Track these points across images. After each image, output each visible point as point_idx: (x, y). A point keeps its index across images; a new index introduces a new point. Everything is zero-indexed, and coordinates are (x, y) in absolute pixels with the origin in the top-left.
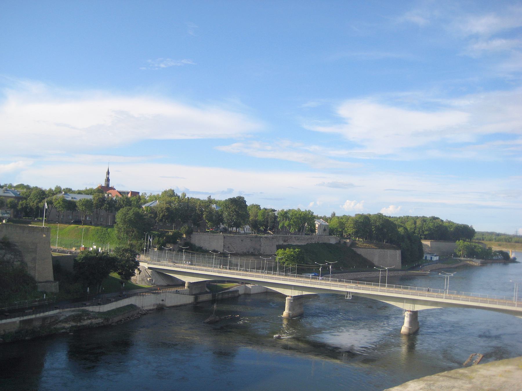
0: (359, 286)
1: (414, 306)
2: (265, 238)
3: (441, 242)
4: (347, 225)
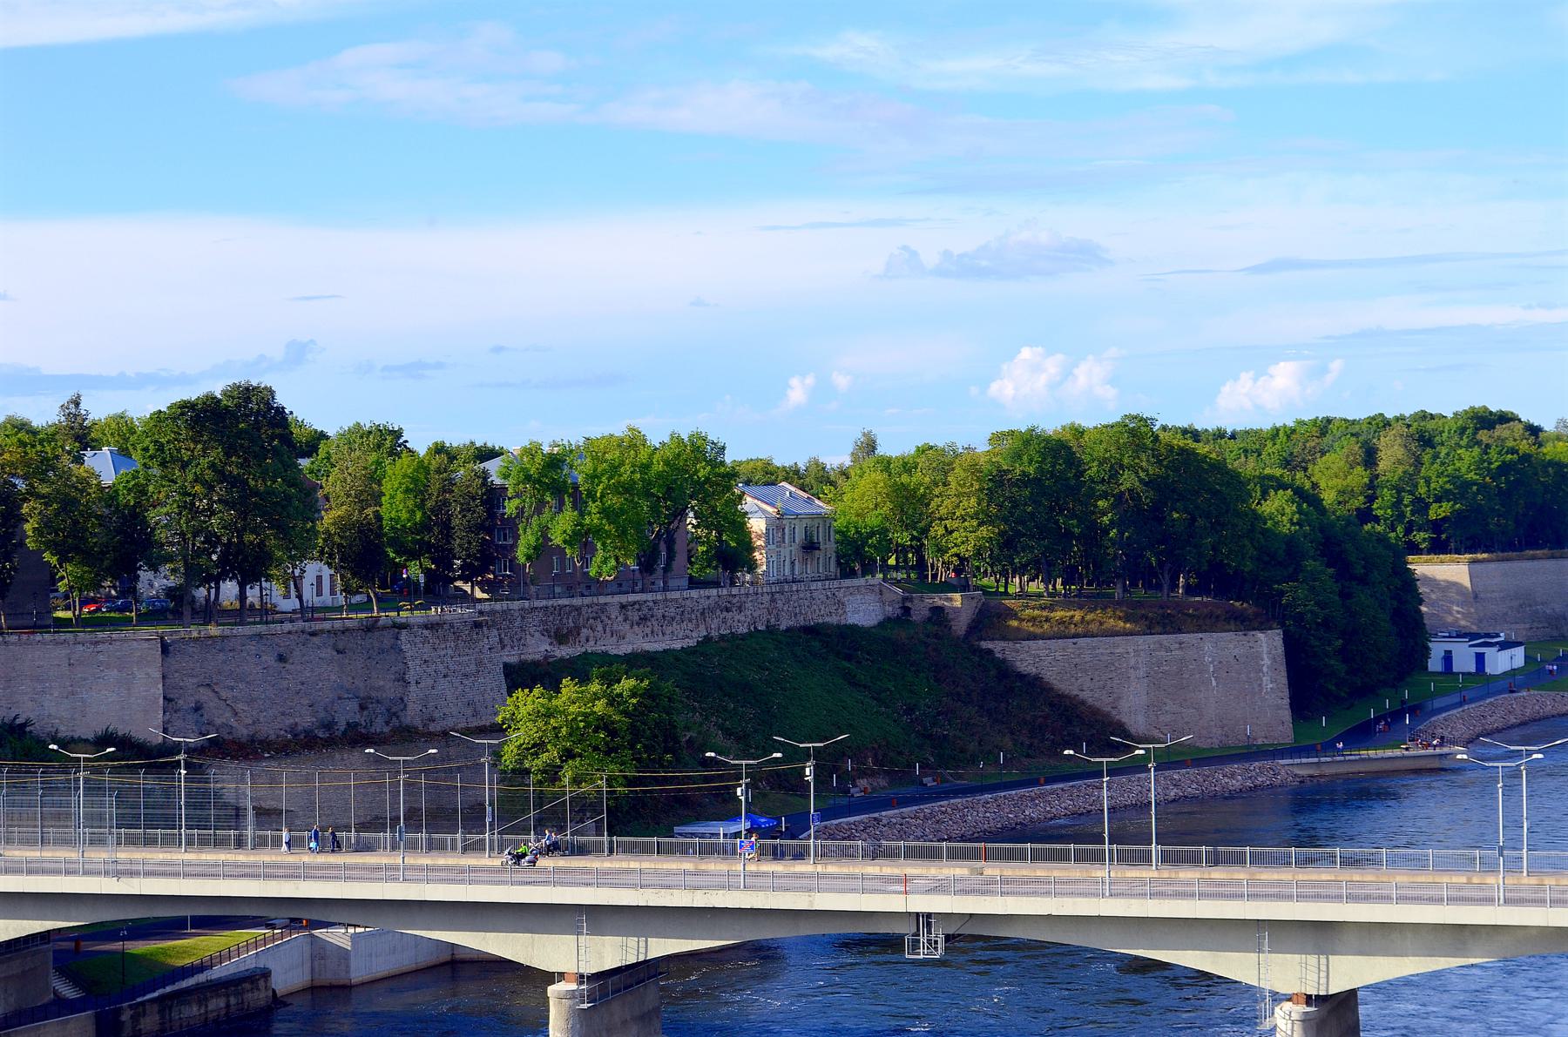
0: (993, 870)
1: (1323, 968)
2: (426, 627)
3: (1534, 558)
4: (942, 505)
